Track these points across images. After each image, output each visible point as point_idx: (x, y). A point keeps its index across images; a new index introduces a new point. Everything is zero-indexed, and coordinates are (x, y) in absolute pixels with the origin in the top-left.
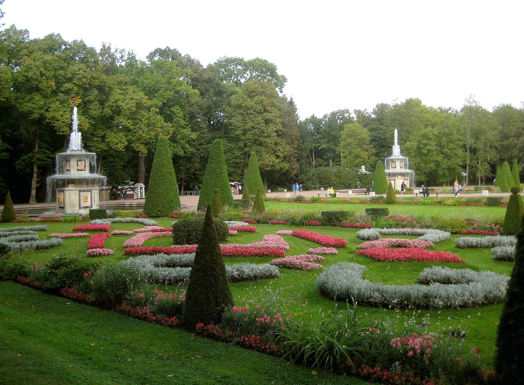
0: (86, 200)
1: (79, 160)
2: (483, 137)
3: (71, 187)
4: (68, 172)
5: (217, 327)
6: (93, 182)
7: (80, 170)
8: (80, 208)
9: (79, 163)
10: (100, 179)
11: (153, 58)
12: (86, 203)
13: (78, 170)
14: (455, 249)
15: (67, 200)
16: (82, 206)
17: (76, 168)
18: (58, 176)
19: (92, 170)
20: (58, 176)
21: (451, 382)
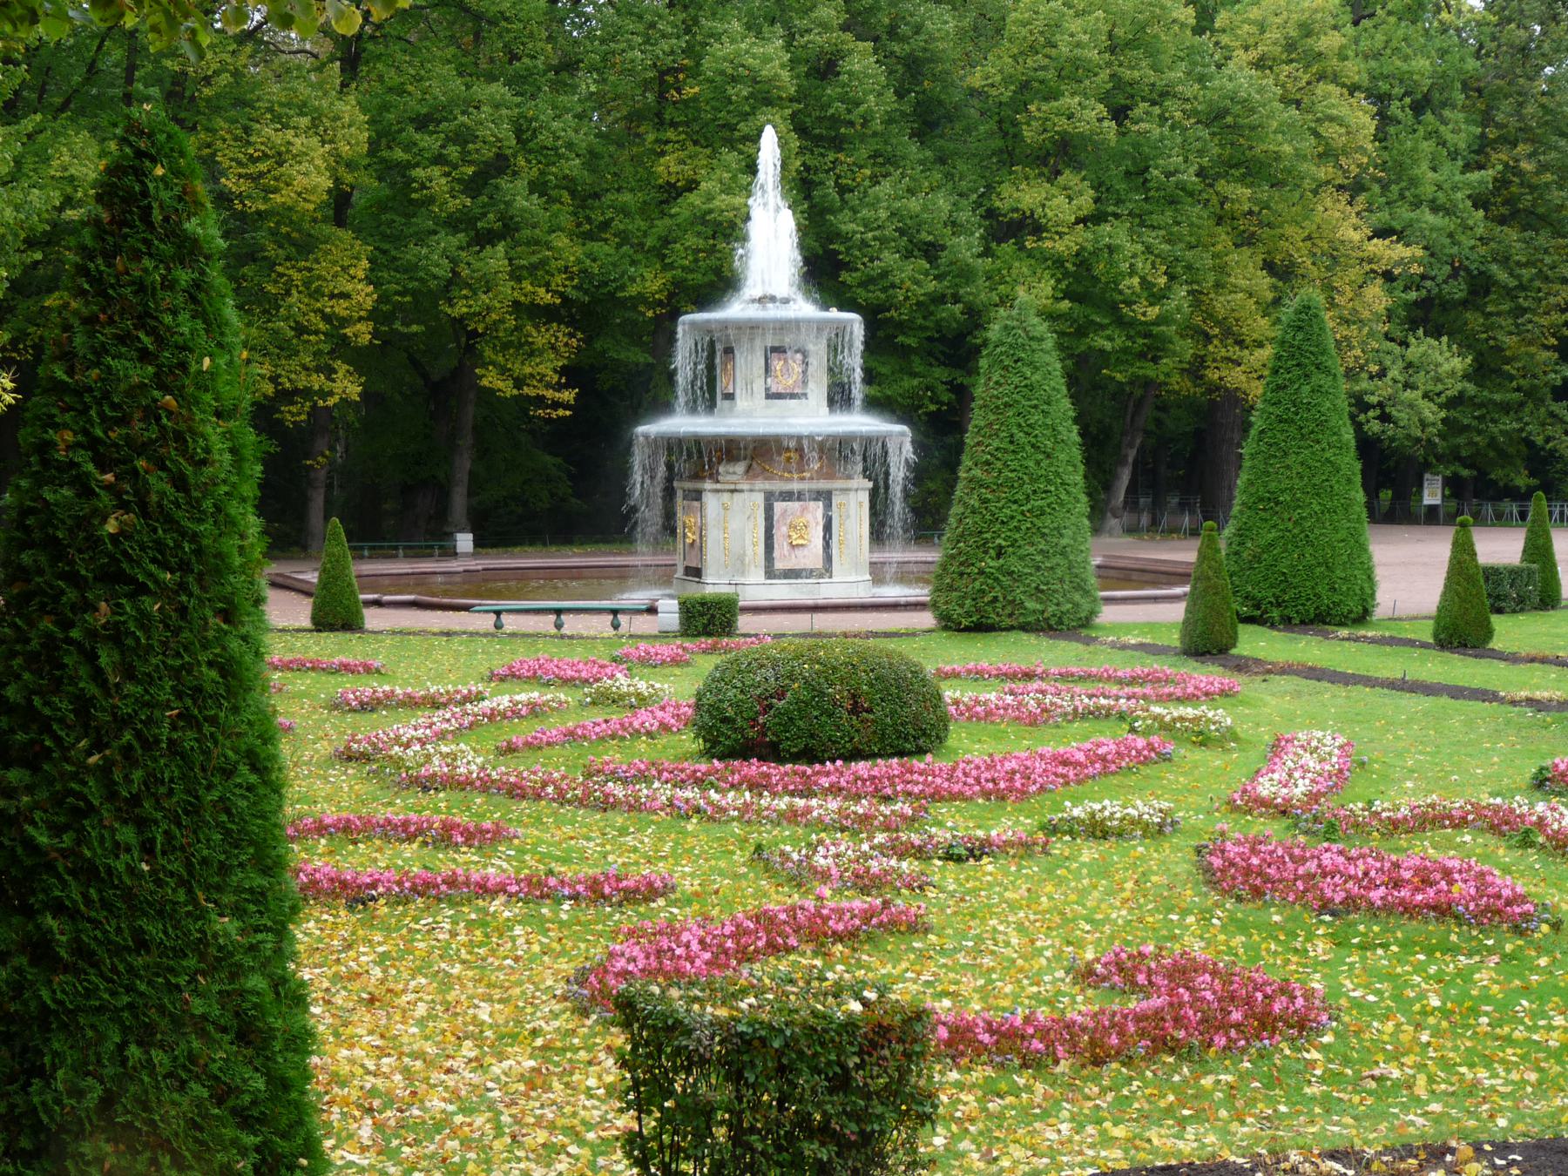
0: (802, 537)
1: (775, 350)
2: (1334, 759)
3: (733, 472)
4: (727, 403)
5: (1060, 974)
6: (836, 451)
7: (779, 396)
8: (770, 573)
9: (777, 364)
10: (868, 441)
11: (1114, 88)
12: (798, 552)
13: (771, 396)
14: (689, 766)
15: (713, 537)
16: (779, 565)
17: (759, 386)
18: (680, 423)
19: (838, 397)
20: (680, 423)
21: (15, 286)
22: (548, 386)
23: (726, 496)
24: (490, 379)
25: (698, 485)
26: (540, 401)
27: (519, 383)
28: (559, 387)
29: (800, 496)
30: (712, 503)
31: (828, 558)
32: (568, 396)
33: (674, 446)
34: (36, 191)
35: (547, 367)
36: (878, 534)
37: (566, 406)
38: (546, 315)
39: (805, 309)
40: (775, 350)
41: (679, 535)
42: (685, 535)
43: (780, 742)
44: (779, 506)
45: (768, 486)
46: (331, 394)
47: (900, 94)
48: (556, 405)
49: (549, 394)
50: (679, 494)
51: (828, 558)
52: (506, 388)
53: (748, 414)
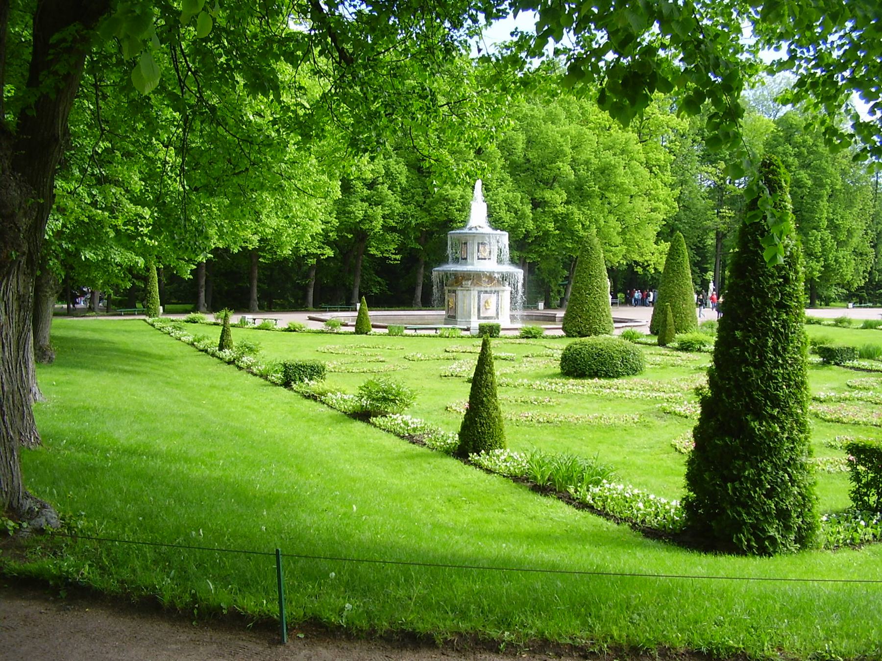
8: (479, 318)
16: (482, 315)
18: (451, 267)
19: (500, 261)
20: (451, 267)
22: (392, 254)
23: (465, 292)
24: (373, 251)
25: (454, 288)
26: (388, 258)
27: (382, 253)
28: (395, 254)
29: (491, 292)
30: (460, 294)
31: (498, 314)
32: (398, 257)
33: (447, 274)
34: (581, 226)
35: (392, 247)
36: (513, 306)
37: (398, 260)
38: (393, 229)
39: (489, 230)
40: (482, 243)
41: (446, 303)
42: (448, 305)
43: (319, 525)
44: (482, 295)
45: (479, 289)
46: (325, 255)
47: (506, 160)
48: (395, 259)
49: (393, 256)
50: (446, 292)
51: (498, 314)
52: (379, 254)
53: (472, 264)
